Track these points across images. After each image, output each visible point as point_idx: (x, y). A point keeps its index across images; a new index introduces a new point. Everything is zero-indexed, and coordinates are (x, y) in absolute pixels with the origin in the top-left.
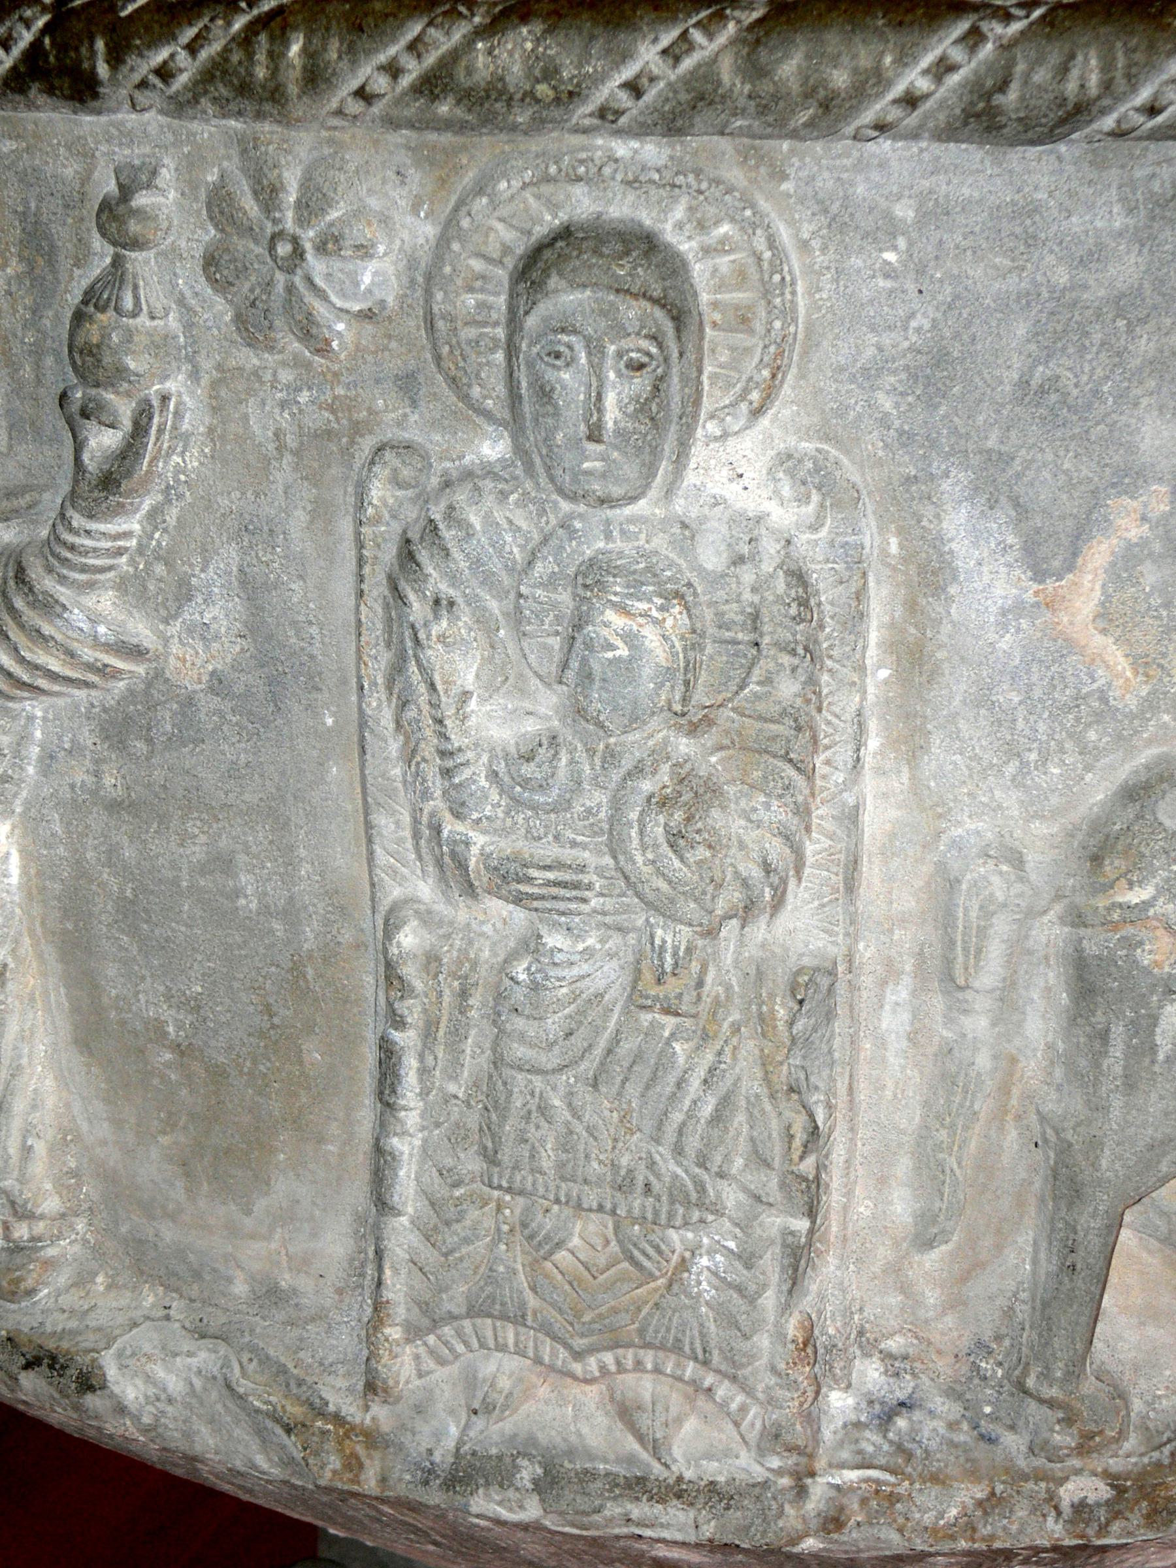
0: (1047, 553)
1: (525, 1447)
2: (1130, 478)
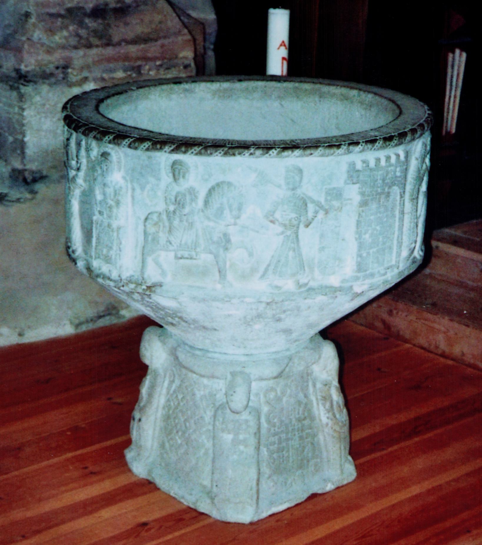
0: (143, 188)
1: (101, 274)
2: (148, 183)
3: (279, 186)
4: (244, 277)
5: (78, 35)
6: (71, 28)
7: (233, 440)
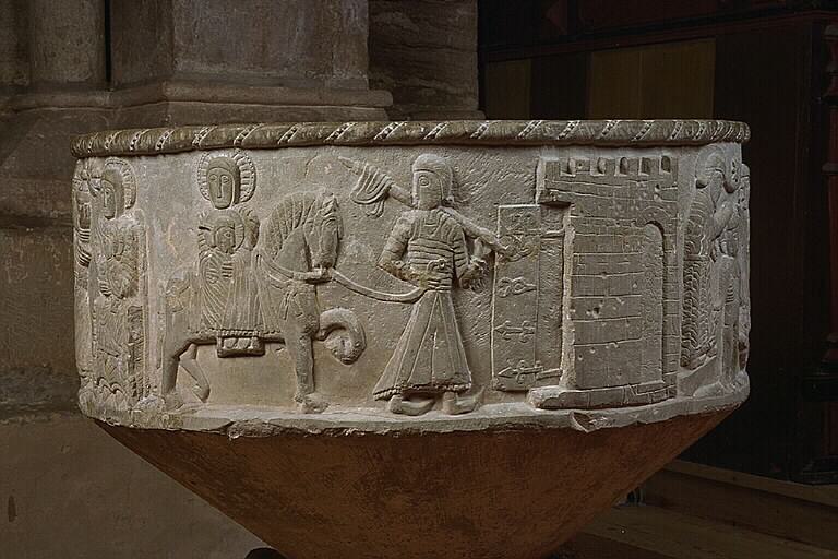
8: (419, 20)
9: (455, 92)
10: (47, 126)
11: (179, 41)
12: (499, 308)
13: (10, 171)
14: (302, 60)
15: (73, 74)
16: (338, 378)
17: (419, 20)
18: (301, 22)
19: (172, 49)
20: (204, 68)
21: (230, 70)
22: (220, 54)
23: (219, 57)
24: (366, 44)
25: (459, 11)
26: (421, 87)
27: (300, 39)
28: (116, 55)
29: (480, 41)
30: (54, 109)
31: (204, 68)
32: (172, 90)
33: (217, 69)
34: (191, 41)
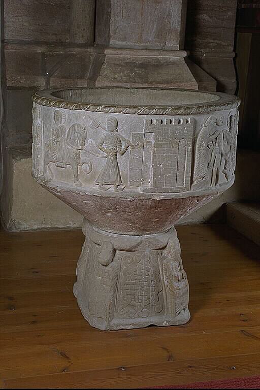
3: (105, 129)
4: (88, 181)
5: (129, 76)
6: (126, 72)
7: (101, 281)
8: (212, 17)
9: (224, 44)
10: (71, 59)
11: (111, 34)
12: (130, 162)
13: (56, 76)
14: (154, 40)
15: (81, 41)
16: (85, 178)
17: (212, 17)
18: (155, 26)
19: (109, 37)
20: (119, 43)
21: (128, 43)
22: (125, 38)
23: (125, 39)
24: (179, 33)
25: (229, 13)
26: (210, 43)
27: (154, 32)
28: (97, 34)
29: (236, 25)
30: (74, 53)
31: (119, 43)
32: (107, 51)
33: (124, 43)
34: (115, 34)
